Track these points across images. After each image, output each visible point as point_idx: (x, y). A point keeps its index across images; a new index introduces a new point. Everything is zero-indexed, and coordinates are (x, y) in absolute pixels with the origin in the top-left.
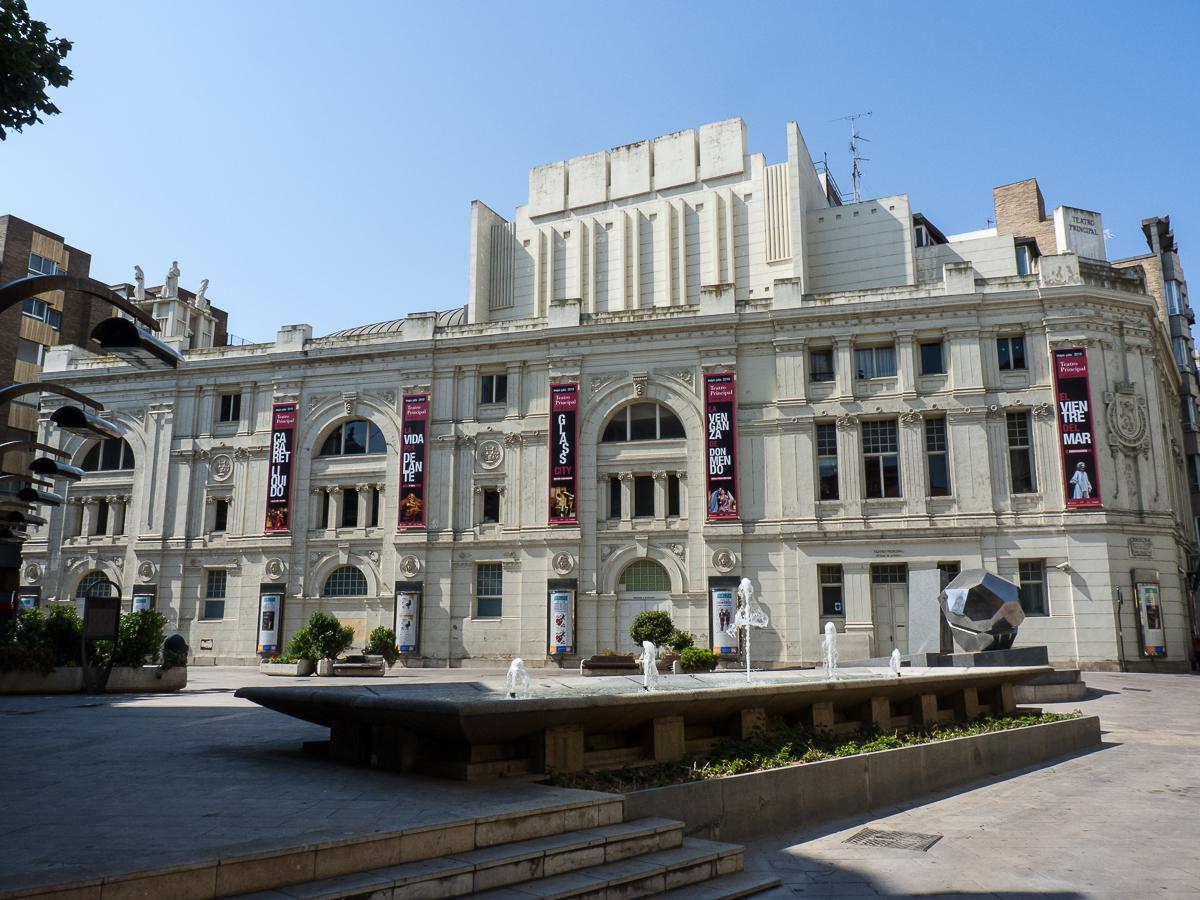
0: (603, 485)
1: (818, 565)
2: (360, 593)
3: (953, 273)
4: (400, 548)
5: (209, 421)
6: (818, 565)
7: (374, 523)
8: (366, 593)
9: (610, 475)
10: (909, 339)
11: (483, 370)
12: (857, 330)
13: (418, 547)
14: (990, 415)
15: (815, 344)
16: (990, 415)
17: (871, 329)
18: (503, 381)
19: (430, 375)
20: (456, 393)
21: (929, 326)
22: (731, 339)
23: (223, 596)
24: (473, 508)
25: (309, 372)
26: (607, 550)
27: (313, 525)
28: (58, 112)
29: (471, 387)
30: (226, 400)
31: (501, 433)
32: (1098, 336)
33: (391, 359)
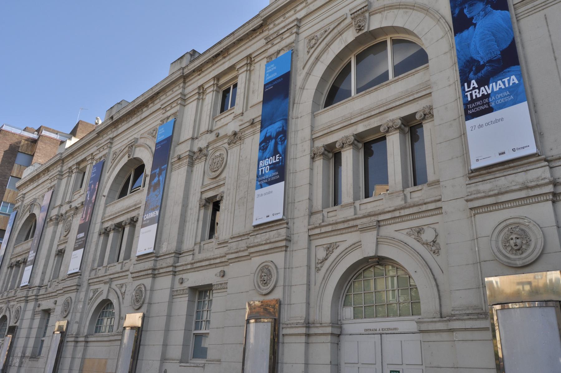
0: (319, 163)
27: (318, 203)
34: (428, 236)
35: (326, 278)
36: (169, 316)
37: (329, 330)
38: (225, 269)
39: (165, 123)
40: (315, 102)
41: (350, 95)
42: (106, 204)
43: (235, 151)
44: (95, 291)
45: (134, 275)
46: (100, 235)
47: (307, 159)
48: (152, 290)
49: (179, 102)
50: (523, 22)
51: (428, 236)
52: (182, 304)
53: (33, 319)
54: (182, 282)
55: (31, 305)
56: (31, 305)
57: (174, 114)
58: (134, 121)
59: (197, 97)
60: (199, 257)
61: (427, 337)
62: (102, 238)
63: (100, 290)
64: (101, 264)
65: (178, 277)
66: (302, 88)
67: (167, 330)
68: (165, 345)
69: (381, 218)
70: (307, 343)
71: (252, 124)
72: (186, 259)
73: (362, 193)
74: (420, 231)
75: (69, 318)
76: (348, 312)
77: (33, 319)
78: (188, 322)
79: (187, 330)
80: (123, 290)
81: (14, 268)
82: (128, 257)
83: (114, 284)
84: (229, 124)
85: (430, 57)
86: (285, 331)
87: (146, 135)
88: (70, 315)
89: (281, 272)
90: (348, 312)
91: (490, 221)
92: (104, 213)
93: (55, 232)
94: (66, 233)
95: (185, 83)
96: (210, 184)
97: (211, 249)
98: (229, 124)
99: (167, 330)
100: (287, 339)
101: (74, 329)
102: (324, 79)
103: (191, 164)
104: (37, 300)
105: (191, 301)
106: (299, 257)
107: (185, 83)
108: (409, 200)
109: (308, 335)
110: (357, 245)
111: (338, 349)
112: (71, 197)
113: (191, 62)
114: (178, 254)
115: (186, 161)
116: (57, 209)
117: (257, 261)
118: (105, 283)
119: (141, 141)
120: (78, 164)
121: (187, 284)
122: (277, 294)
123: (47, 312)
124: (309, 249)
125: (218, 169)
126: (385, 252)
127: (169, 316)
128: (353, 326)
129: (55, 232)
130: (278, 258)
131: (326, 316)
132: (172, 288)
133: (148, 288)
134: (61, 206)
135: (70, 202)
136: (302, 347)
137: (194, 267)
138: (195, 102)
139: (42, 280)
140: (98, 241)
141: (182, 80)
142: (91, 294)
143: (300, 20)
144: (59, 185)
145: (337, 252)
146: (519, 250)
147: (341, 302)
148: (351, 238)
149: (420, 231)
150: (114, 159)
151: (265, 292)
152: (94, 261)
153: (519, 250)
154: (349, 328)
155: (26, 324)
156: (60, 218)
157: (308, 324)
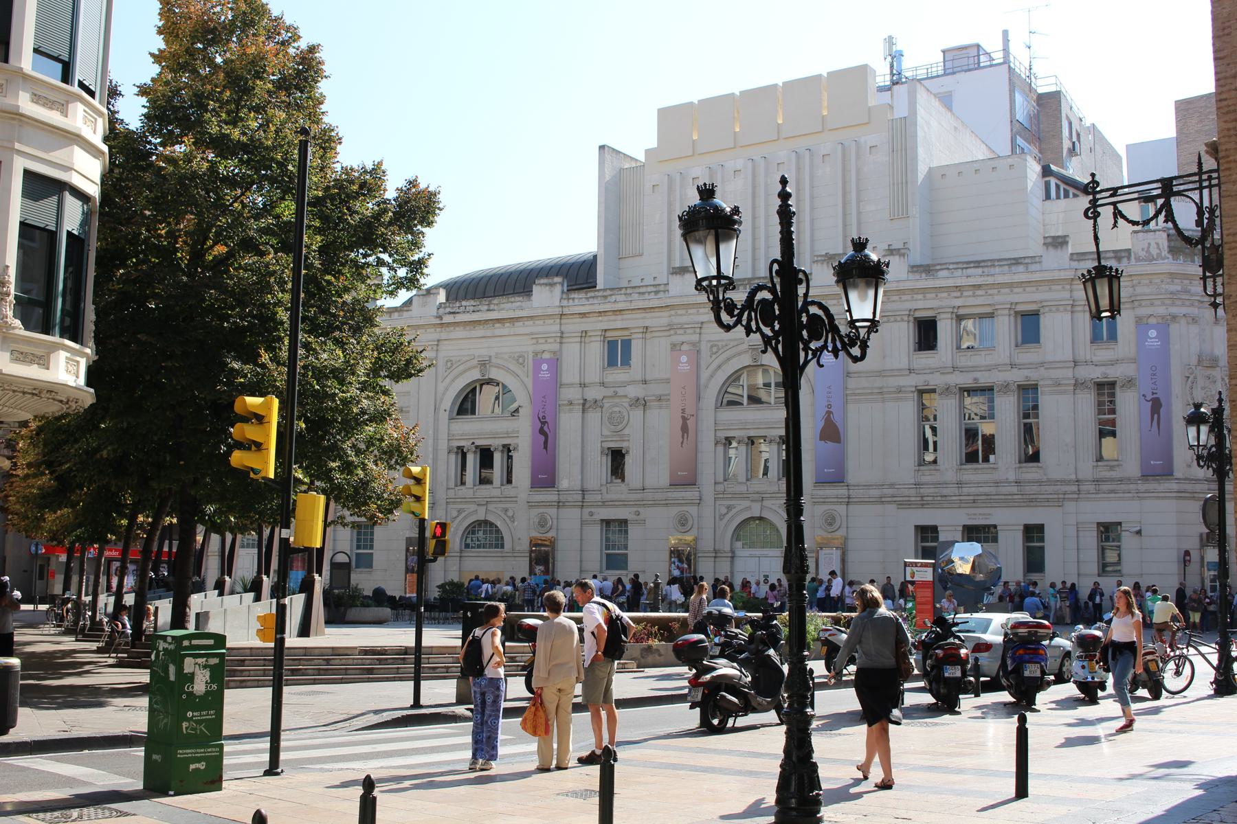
0: (453, 457)
1: (917, 527)
2: (497, 547)
3: (1051, 248)
4: (531, 505)
5: (949, 348)
6: (917, 527)
7: (509, 481)
8: (502, 547)
9: (458, 448)
10: (1006, 312)
11: (608, 334)
12: (958, 302)
13: (548, 505)
14: (1078, 385)
15: (1020, 308)
16: (1078, 385)
17: (971, 301)
18: (627, 344)
19: (1069, 308)
20: (582, 355)
21: (1026, 299)
22: (1066, 295)
23: (372, 547)
24: (600, 466)
25: (444, 336)
26: (724, 510)
27: (452, 484)
28: (890, 41)
29: (596, 351)
30: (612, 345)
31: (626, 396)
32: (1184, 310)
33: (521, 324)
34: (510, 513)
38: (641, 510)
46: (716, 444)
51: (510, 513)
54: (591, 514)
63: (738, 508)
74: (506, 510)
89: (844, 519)
90: (739, 544)
91: (822, 508)
106: (708, 511)
110: (749, 508)
121: (598, 517)
126: (491, 518)
130: (693, 510)
131: (727, 548)
133: (555, 516)
146: (831, 524)
148: (746, 503)
149: (506, 510)
153: (831, 524)
154: (739, 553)
157: (716, 551)
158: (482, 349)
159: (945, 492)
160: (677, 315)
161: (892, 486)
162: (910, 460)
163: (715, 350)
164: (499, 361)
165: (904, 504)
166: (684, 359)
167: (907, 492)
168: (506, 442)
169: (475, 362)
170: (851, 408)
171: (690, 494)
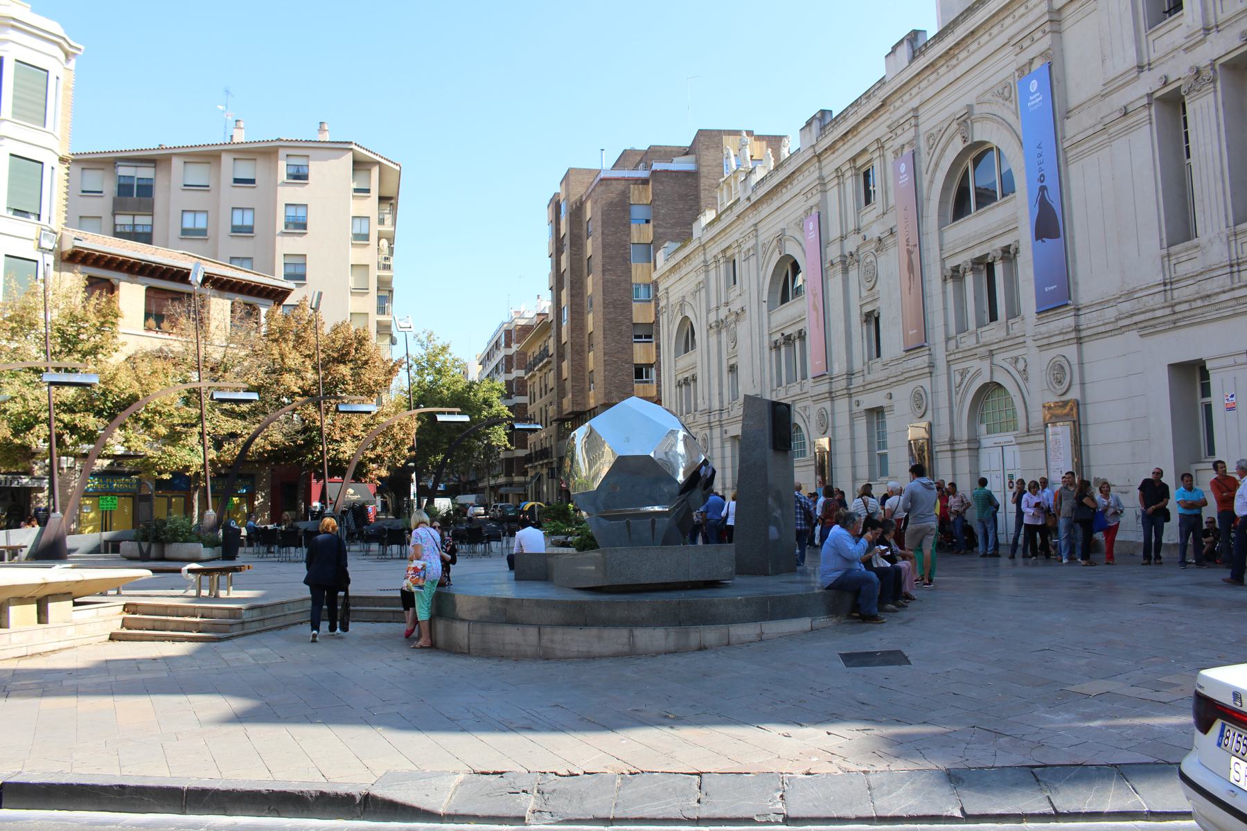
1: (1172, 366)
11: (859, 163)
34: (1021, 366)
35: (962, 401)
36: (853, 439)
37: (966, 446)
39: (1026, 72)
40: (941, 215)
41: (995, 199)
42: (769, 311)
43: (882, 259)
44: (963, 373)
45: (1039, 343)
46: (945, 280)
47: (939, 281)
48: (833, 414)
49: (1047, 28)
50: (1071, 167)
52: (861, 425)
53: (723, 447)
55: (717, 432)
56: (717, 432)
57: (910, 143)
58: (776, 203)
59: (836, 181)
60: (869, 378)
61: (1025, 447)
62: (774, 352)
63: (972, 371)
64: (962, 328)
65: (854, 399)
66: (929, 199)
67: (853, 453)
68: (854, 467)
69: (993, 347)
70: (953, 458)
71: (1125, 114)
72: (858, 381)
73: (987, 317)
74: (1016, 360)
75: (929, 417)
76: (983, 428)
77: (723, 447)
78: (870, 443)
79: (870, 451)
80: (1021, 366)
81: (783, 349)
82: (804, 377)
83: (998, 359)
84: (874, 222)
85: (1017, 188)
86: (937, 449)
87: (988, 96)
88: (929, 413)
89: (1076, 368)
92: (769, 323)
93: (719, 343)
94: (870, 285)
95: (819, 161)
96: (866, 297)
97: (878, 372)
98: (874, 222)
99: (853, 453)
100: (940, 455)
101: (942, 434)
102: (946, 188)
103: (845, 271)
104: (850, 396)
105: (869, 423)
107: (819, 161)
108: (982, 340)
109: (953, 451)
111: (978, 460)
112: (727, 297)
113: (913, 58)
114: (850, 375)
115: (839, 267)
116: (838, 244)
117: (912, 385)
118: (981, 358)
119: (978, 110)
120: (724, 251)
121: (730, 434)
122: (1074, 394)
123: (877, 413)
124: (949, 374)
125: (872, 277)
127: (853, 439)
128: (987, 441)
129: (719, 343)
130: (926, 382)
131: (963, 433)
132: (850, 411)
134: (843, 238)
135: (727, 304)
136: (949, 461)
137: (866, 389)
138: (836, 188)
139: (721, 402)
140: (944, 293)
141: (816, 159)
142: (958, 379)
143: (916, 109)
144: (707, 278)
145: (968, 376)
147: (978, 420)
149: (1016, 360)
150: (765, 253)
151: (1060, 392)
152: (771, 380)
155: (717, 453)
156: (846, 262)
158: (953, 104)
159: (1210, 287)
160: (896, 109)
161: (1129, 295)
162: (1151, 239)
163: (931, 142)
164: (985, 109)
165: (1148, 327)
166: (1034, 86)
167: (1151, 302)
168: (977, 253)
169: (954, 126)
170: (1074, 170)
171: (921, 361)
